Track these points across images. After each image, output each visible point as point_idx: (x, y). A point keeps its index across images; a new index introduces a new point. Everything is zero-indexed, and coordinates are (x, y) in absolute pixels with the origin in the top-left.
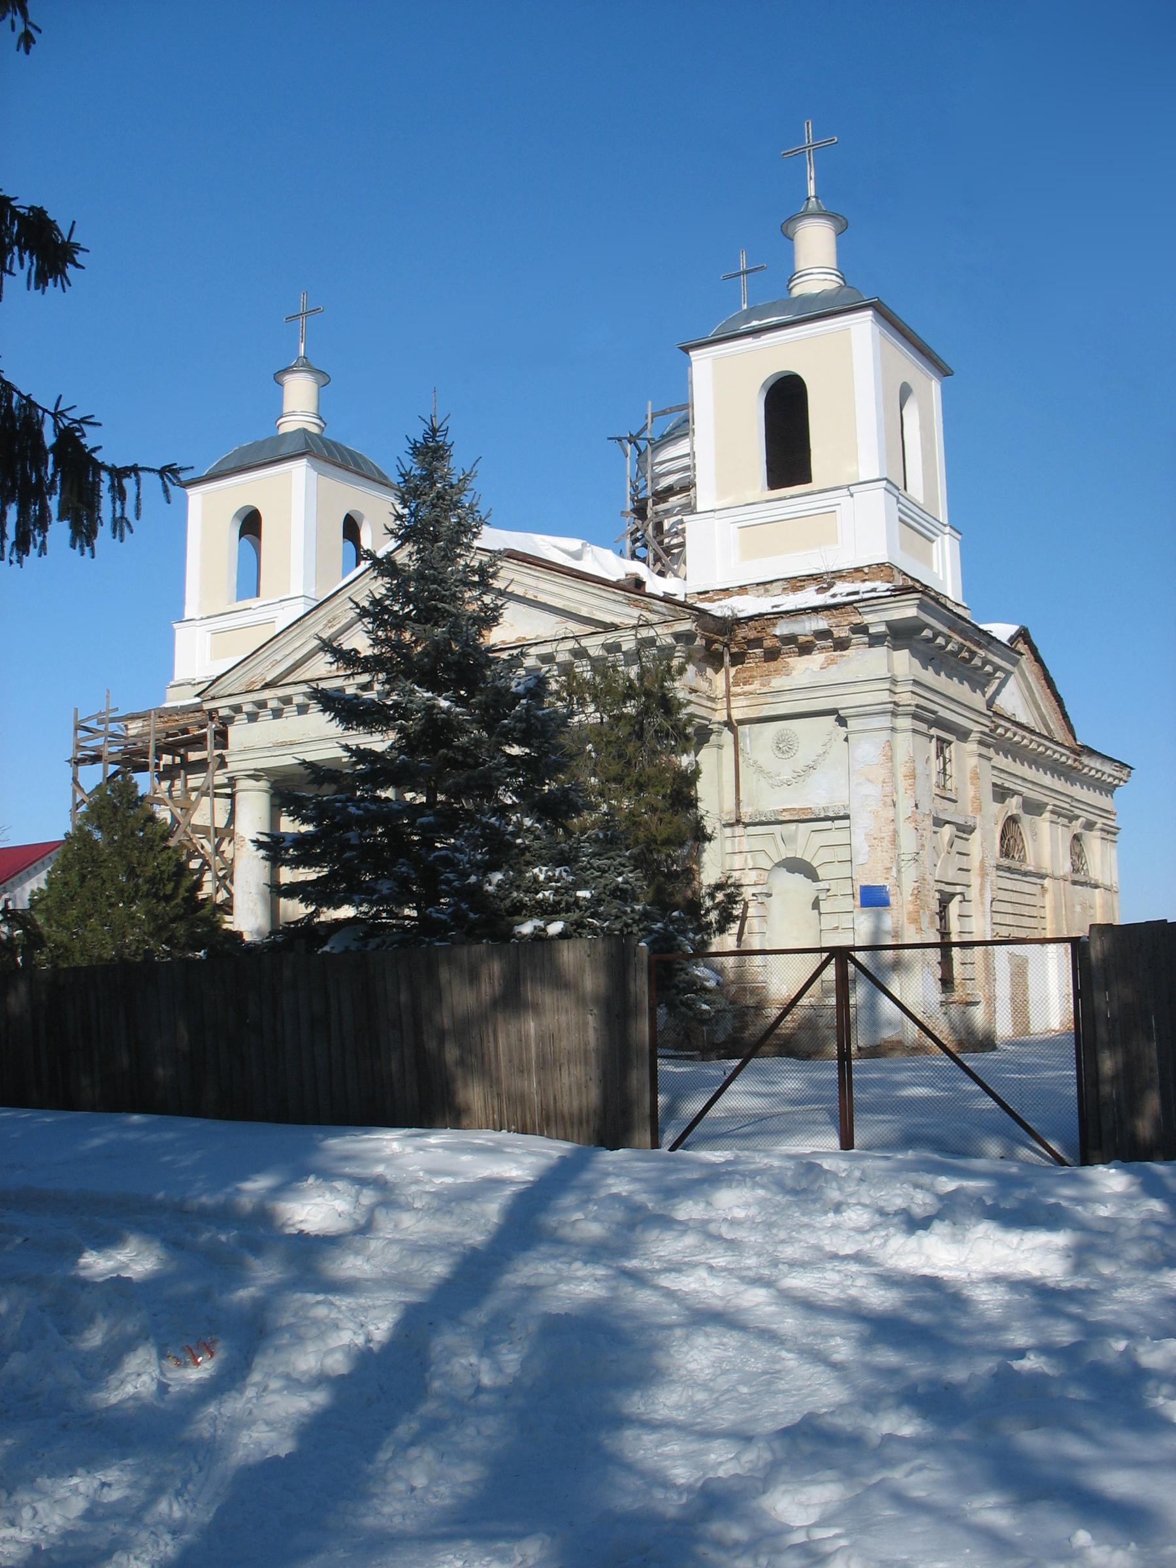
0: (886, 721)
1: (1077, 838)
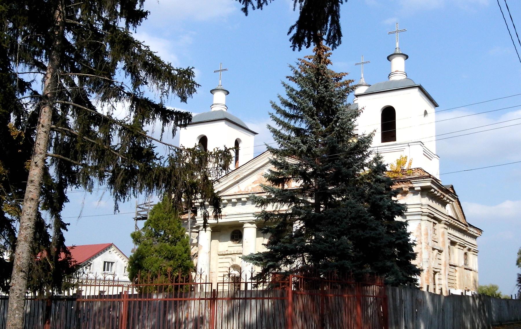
0: (419, 217)
1: (466, 254)
